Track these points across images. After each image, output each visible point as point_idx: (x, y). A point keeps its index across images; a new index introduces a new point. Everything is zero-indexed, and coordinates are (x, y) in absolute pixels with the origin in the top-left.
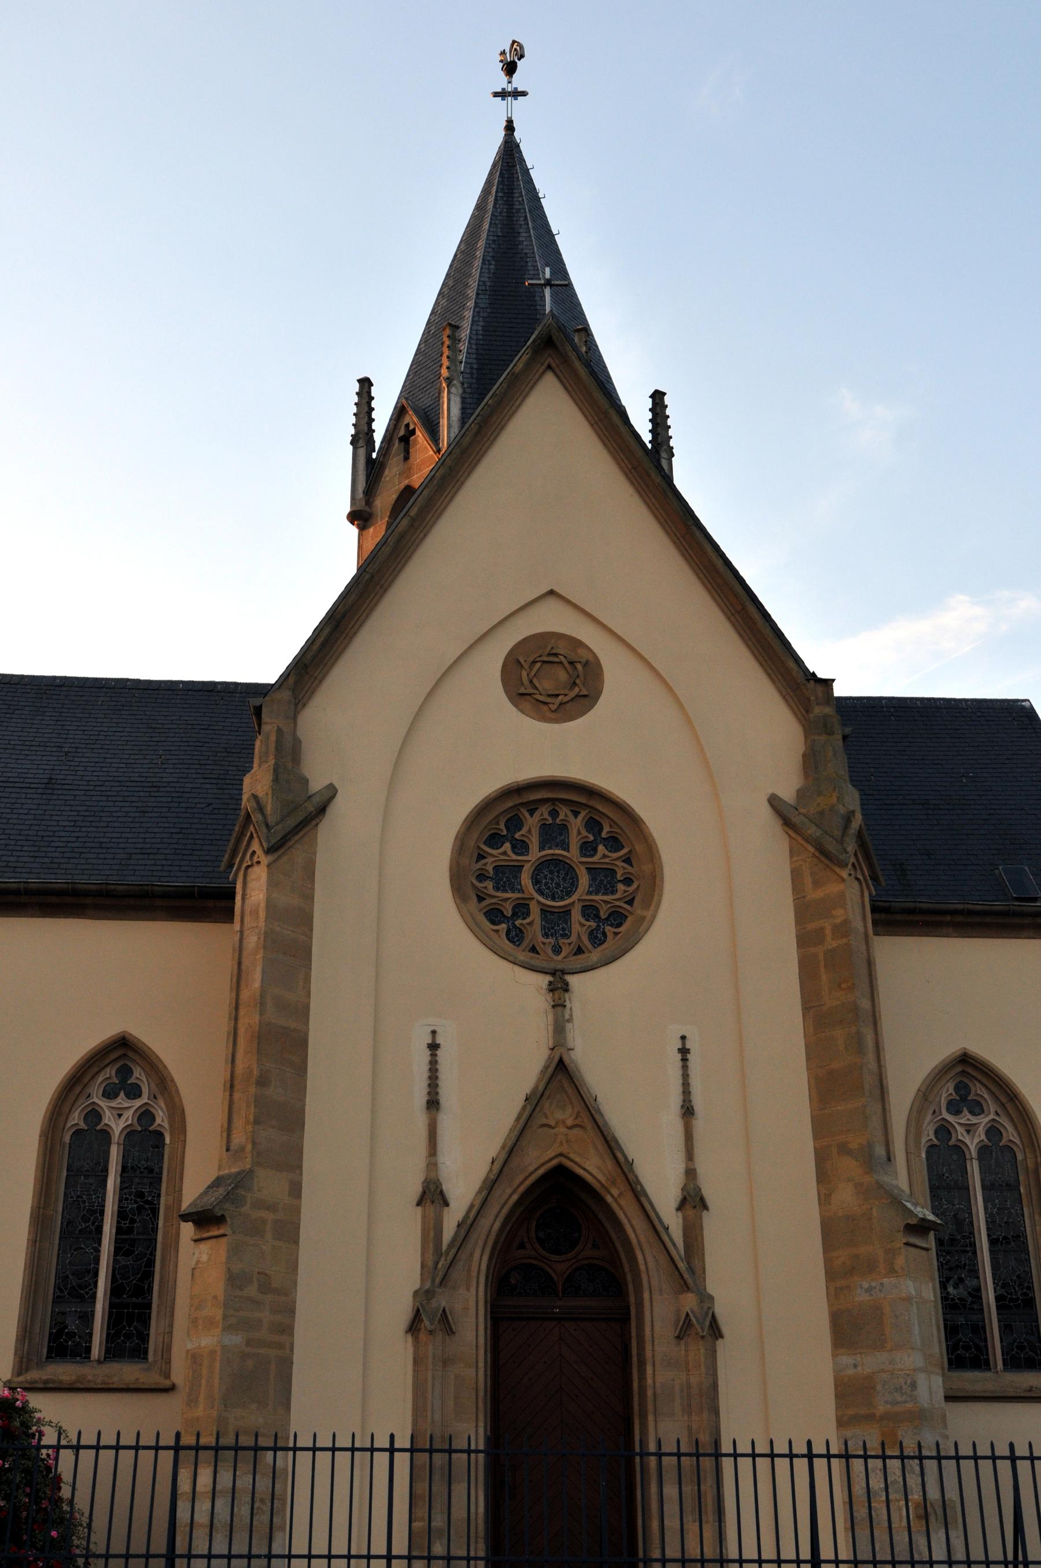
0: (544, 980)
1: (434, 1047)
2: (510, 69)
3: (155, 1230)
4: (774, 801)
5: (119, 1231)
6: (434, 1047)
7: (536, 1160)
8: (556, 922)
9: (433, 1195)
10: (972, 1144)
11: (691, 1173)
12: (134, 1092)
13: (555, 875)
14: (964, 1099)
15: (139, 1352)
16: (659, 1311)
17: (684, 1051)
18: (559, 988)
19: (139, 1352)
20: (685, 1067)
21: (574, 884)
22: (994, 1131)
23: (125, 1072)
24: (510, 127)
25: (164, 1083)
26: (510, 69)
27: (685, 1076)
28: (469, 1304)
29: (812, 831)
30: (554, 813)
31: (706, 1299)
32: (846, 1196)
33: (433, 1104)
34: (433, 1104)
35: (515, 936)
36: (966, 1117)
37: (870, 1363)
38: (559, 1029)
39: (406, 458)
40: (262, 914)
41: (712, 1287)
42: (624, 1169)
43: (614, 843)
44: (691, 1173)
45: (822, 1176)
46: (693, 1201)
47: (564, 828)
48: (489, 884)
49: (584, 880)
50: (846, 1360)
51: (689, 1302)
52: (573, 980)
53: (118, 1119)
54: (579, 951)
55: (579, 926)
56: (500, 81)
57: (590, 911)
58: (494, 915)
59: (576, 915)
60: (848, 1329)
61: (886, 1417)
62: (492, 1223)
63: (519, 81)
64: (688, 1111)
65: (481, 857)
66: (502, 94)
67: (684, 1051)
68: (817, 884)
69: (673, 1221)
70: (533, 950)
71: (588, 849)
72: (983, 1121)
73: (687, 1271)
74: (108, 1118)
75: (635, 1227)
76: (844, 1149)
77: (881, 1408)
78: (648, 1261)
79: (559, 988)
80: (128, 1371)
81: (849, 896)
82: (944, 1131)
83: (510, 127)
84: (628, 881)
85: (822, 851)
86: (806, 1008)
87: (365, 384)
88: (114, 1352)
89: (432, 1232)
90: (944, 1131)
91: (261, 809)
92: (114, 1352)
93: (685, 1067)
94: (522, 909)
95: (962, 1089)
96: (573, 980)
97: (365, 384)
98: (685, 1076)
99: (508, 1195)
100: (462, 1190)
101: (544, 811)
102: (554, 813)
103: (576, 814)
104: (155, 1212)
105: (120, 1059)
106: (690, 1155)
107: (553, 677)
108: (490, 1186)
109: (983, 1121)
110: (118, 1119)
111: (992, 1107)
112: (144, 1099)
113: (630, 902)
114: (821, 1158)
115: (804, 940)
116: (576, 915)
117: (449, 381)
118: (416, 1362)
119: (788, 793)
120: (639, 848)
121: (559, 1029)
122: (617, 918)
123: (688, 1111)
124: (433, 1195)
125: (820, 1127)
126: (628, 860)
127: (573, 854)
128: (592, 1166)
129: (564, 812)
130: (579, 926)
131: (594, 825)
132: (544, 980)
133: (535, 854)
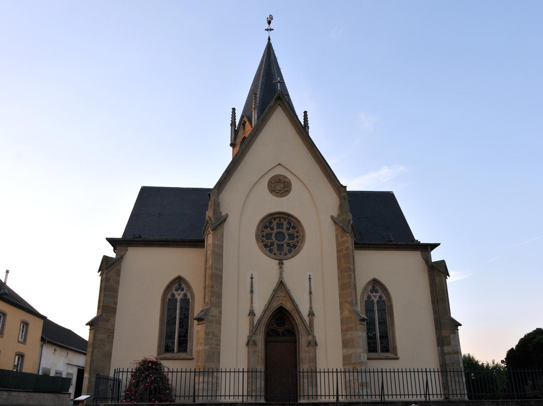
0: (277, 262)
1: (252, 278)
2: (269, 23)
3: (188, 322)
4: (332, 217)
5: (180, 323)
6: (252, 278)
7: (275, 305)
8: (280, 247)
9: (252, 313)
10: (375, 300)
11: (311, 308)
12: (182, 290)
13: (280, 236)
14: (374, 290)
15: (185, 351)
16: (303, 340)
17: (310, 279)
18: (281, 263)
19: (185, 351)
20: (310, 282)
21: (285, 238)
22: (380, 297)
23: (180, 285)
24: (269, 39)
25: (189, 287)
26: (269, 23)
27: (310, 284)
28: (260, 339)
29: (341, 224)
30: (280, 220)
31: (314, 337)
32: (346, 313)
33: (252, 292)
34: (252, 292)
35: (271, 251)
36: (374, 294)
37: (350, 351)
38: (281, 274)
39: (244, 127)
40: (211, 246)
41: (315, 334)
42: (296, 307)
43: (294, 228)
44: (311, 308)
45: (341, 308)
46: (311, 314)
47: (282, 224)
48: (265, 238)
49: (287, 237)
50: (345, 351)
51: (310, 338)
52: (284, 262)
53: (179, 296)
54: (286, 254)
55: (286, 248)
56: (267, 26)
57: (288, 245)
58: (266, 246)
59: (285, 245)
60: (346, 344)
61: (354, 363)
62: (265, 320)
63: (272, 26)
64: (310, 293)
65: (263, 231)
66: (267, 30)
67: (310, 279)
68: (342, 238)
69: (307, 319)
70: (275, 254)
71: (288, 229)
72: (378, 295)
73: (310, 330)
74: (176, 296)
75: (298, 321)
76: (346, 302)
77: (353, 361)
78: (301, 328)
79: (281, 263)
80: (183, 355)
81: (349, 240)
82: (369, 297)
83: (269, 39)
84: (297, 237)
85: (343, 230)
86: (338, 268)
87: (234, 109)
88: (179, 351)
89: (252, 322)
90: (369, 297)
91: (211, 220)
92: (179, 351)
93: (310, 282)
94: (272, 244)
95: (374, 287)
96: (284, 262)
97: (234, 109)
98: (310, 284)
99: (269, 314)
100: (258, 312)
101: (277, 220)
102: (280, 220)
103: (285, 220)
104: (188, 318)
105: (179, 282)
106: (311, 303)
107: (280, 186)
108: (265, 311)
109: (378, 295)
110: (179, 296)
111: (380, 291)
112: (185, 291)
113: (298, 242)
114: (341, 304)
115: (338, 252)
116: (285, 245)
117: (254, 108)
118: (248, 352)
119: (335, 215)
120: (300, 229)
121: (281, 274)
122: (295, 246)
123: (310, 293)
124: (252, 313)
125: (341, 296)
126: (297, 232)
127: (284, 231)
128: (288, 306)
129: (282, 220)
130: (286, 248)
131: (289, 223)
132: (277, 262)
133: (275, 231)
